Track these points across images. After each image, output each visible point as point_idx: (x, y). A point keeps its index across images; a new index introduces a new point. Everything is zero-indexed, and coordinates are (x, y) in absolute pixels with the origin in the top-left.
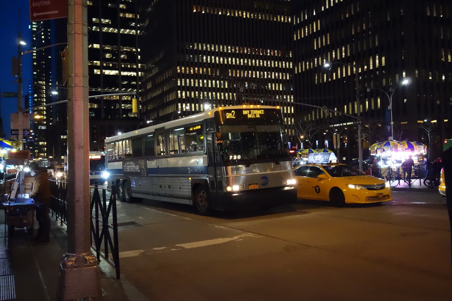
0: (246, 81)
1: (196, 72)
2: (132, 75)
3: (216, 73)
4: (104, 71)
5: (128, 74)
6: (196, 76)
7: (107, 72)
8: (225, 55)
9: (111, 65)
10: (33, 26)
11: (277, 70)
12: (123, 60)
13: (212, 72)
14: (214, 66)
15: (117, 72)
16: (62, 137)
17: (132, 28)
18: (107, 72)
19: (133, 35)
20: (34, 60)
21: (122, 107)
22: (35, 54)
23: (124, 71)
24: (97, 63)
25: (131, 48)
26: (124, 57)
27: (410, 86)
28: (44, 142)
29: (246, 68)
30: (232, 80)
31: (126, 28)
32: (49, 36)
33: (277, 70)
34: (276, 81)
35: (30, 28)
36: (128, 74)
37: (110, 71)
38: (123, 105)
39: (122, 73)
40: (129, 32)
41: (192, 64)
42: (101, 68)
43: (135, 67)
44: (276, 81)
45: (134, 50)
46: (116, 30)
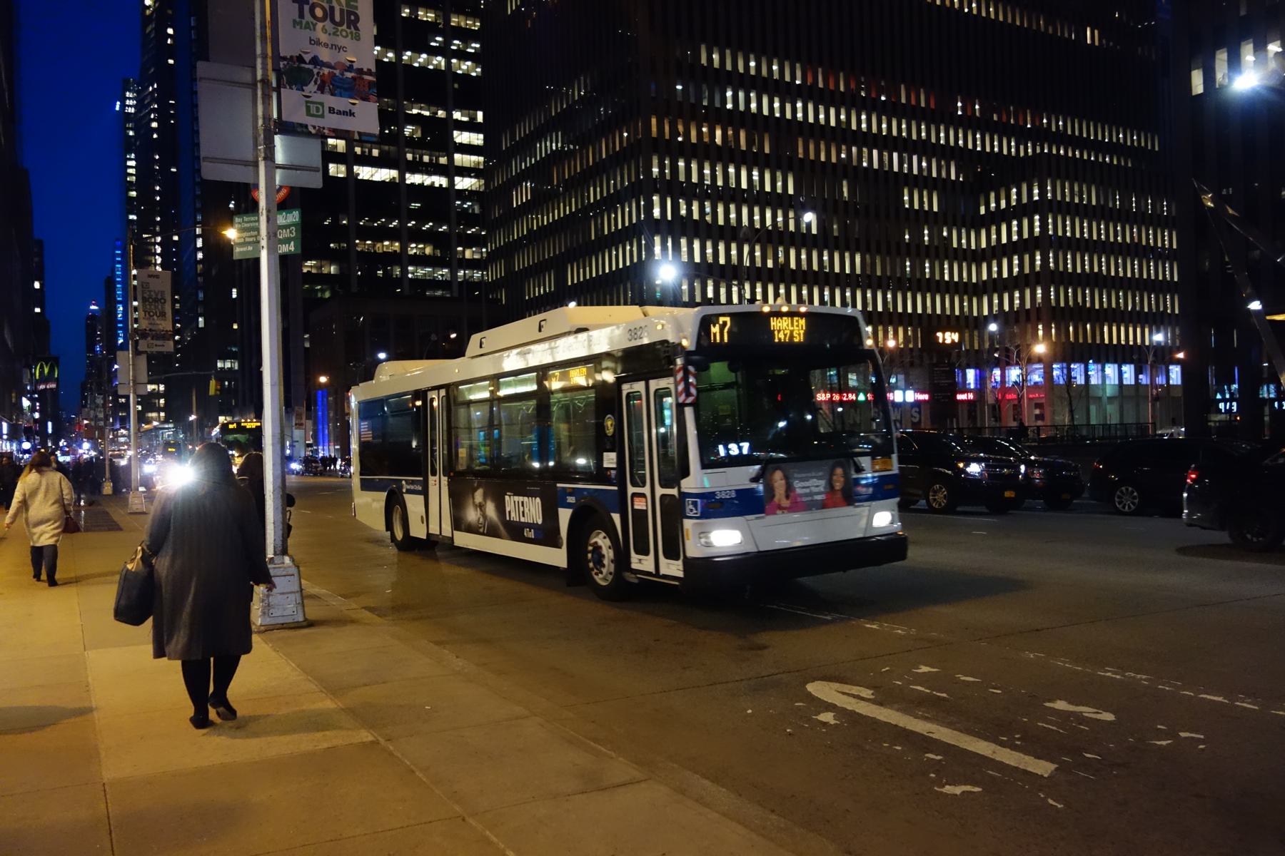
0: (845, 177)
1: (706, 140)
2: (437, 185)
3: (761, 147)
4: (356, 168)
5: (427, 180)
6: (705, 152)
7: (365, 173)
8: (787, 92)
9: (375, 153)
10: (128, 102)
11: (925, 149)
12: (411, 143)
13: (750, 142)
14: (755, 123)
15: (394, 173)
16: (220, 365)
17: (433, 52)
18: (365, 173)
19: (437, 70)
20: (130, 186)
21: (408, 272)
22: (154, 125)
23: (413, 172)
24: (336, 146)
25: (433, 109)
26: (413, 132)
27: (325, 384)
28: (158, 383)
29: (843, 135)
30: (807, 172)
31: (418, 50)
32: (172, 116)
33: (925, 149)
34: (922, 182)
35: (117, 108)
36: (427, 180)
37: (374, 170)
38: (410, 268)
39: (407, 175)
40: (429, 62)
41: (694, 114)
42: (348, 159)
43: (443, 160)
44: (922, 182)
45: (441, 114)
46: (391, 55)
